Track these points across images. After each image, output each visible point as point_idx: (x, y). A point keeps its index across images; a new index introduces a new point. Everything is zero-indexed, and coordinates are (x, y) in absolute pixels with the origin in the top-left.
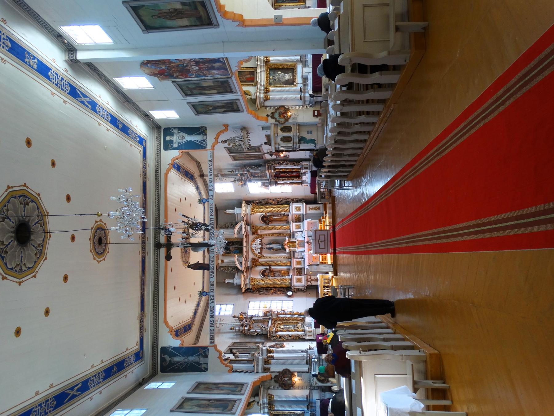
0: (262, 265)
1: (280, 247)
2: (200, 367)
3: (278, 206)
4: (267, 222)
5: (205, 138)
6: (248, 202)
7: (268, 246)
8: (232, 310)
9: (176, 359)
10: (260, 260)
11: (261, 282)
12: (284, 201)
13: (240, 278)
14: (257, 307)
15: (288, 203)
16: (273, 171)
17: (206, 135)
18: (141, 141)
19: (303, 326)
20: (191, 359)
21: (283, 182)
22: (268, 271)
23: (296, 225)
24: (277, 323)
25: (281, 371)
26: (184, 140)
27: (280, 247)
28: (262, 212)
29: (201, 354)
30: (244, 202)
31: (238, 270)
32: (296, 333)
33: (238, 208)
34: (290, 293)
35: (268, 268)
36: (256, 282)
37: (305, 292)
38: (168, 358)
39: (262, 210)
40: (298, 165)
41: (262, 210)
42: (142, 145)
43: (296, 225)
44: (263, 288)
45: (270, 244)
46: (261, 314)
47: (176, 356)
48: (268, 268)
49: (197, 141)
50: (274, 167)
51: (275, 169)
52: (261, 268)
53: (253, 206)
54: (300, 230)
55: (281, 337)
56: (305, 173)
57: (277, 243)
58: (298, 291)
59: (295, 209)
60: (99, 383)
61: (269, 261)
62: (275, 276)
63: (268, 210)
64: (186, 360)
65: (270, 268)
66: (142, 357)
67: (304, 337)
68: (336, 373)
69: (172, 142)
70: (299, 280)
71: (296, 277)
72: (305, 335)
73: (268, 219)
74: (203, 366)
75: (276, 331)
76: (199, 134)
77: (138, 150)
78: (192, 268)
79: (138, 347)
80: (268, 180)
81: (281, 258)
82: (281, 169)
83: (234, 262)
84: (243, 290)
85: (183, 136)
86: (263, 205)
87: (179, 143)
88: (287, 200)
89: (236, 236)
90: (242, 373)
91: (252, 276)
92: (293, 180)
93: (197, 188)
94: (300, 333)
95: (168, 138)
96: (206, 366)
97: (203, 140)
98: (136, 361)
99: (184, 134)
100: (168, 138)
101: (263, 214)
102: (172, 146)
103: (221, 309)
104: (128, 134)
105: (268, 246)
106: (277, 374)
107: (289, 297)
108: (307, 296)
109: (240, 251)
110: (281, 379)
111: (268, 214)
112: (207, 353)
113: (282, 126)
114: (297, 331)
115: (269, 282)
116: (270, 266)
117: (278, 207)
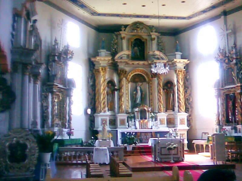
0: (120, 81)
1: (138, 101)
6: (187, 67)
7: (139, 88)
11: (102, 79)
12: (189, 106)
13: (106, 56)
14: (76, 72)
15: (187, 110)
27: (138, 101)
28: (178, 81)
32: (50, 117)
34: (89, 111)
36: (102, 73)
37: (90, 129)
43: (164, 119)
44: (94, 82)
52: (116, 80)
55: (46, 97)
57: (143, 99)
58: (91, 120)
61: (124, 90)
62: (108, 95)
65: (117, 90)
67: (45, 126)
68: (205, 171)
70: (104, 123)
72: (48, 127)
73: (169, 88)
81: (126, 103)
83: (122, 50)
84: (93, 59)
88: (190, 110)
89: (151, 53)
93: (204, 11)
94: (50, 121)
106: (9, 83)
107: (86, 112)
108: (87, 131)
109: (135, 58)
114: (53, 118)
115: (102, 88)
116: (119, 90)
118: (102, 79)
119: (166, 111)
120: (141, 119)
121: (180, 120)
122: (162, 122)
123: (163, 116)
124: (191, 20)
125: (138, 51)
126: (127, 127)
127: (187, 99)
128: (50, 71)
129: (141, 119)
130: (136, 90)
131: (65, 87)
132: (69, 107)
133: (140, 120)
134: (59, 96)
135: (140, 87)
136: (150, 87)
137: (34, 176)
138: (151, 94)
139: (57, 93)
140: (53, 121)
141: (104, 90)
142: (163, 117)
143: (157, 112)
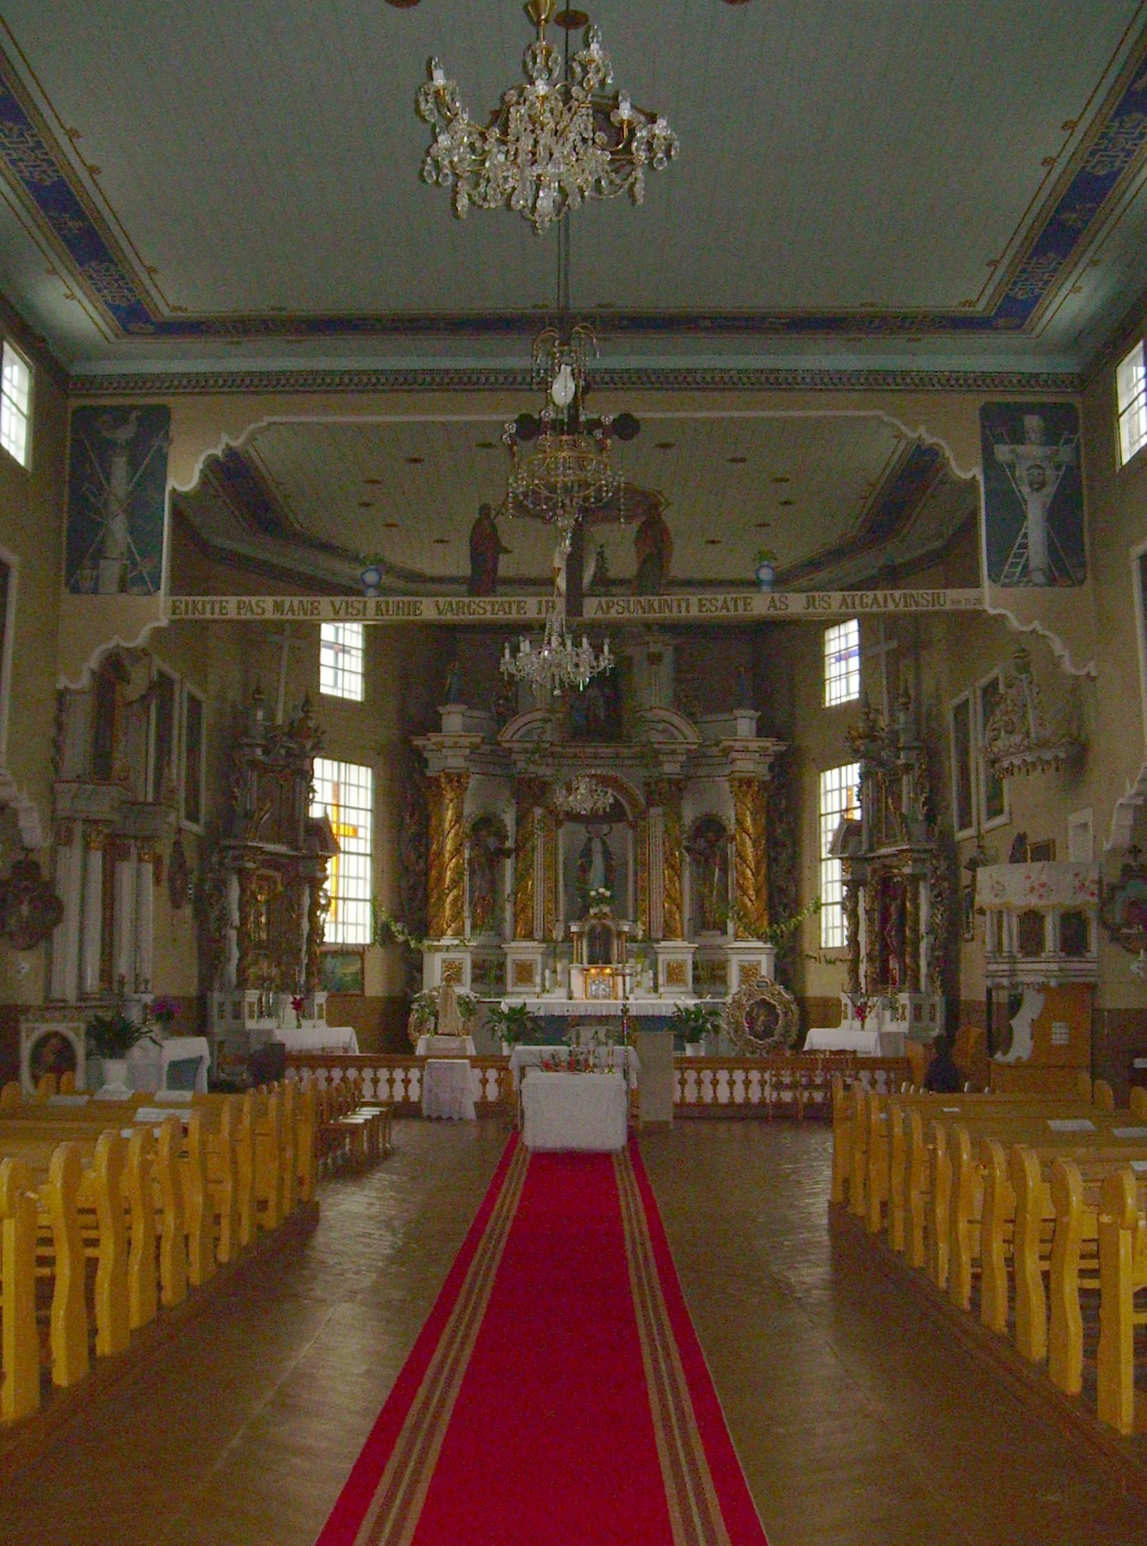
0: (519, 822)
2: (87, 562)
3: (764, 892)
4: (701, 843)
5: (1039, 577)
7: (597, 846)
8: (338, 693)
9: (120, 465)
10: (538, 812)
16: (907, 870)
17: (1052, 581)
18: (1014, 312)
19: (263, 982)
20: (118, 527)
21: (861, 912)
22: (492, 842)
23: (680, 966)
24: (278, 876)
25: (60, 892)
26: (1026, 490)
28: (740, 822)
29: (135, 565)
30: (782, 748)
31: (502, 719)
33: (759, 721)
35: (509, 844)
36: (449, 795)
38: (124, 434)
39: (749, 821)
40: (930, 977)
41: (749, 821)
42: (999, 314)
43: (680, 966)
45: (607, 856)
46: (316, 812)
47: (134, 463)
48: (509, 844)
49: (1024, 546)
50: (923, 877)
51: (915, 879)
53: (764, 786)
54: (661, 980)
56: (892, 1006)
59: (748, 956)
60: (13, 162)
63: (747, 848)
64: (114, 507)
66: (129, 333)
69: (1018, 437)
70: (452, 975)
71: (466, 960)
74: (87, 572)
75: (242, 873)
76: (1052, 550)
77: (972, 290)
78: (478, 525)
79: (167, 313)
80: (871, 848)
82: (917, 907)
84: (418, 742)
85: (1043, 485)
86: (769, 831)
87: (1012, 467)
90: (52, 732)
91: (473, 782)
92: (870, 957)
95: (1033, 422)
96: (87, 584)
97: (1026, 571)
98: (115, 308)
99: (1050, 490)
100: (1033, 422)
101: (732, 827)
102: (999, 440)
103: (344, 649)
104: (1039, 251)
105: (597, 846)
106: (45, 875)
110: (26, 889)
111: (731, 849)
112: (135, 590)
113: (1091, 915)
115: (449, 846)
117: (758, 891)
118: (450, 813)
119: (696, 934)
120: (592, 961)
121: (742, 968)
122: (674, 975)
123: (678, 950)
124: (151, 875)
125: (601, 702)
126: (538, 989)
127: (782, 891)
128: (236, 798)
129: (592, 961)
130: (587, 853)
131: (298, 849)
132: (310, 921)
133: (586, 966)
134: (275, 882)
135: (604, 843)
136: (641, 841)
137: (380, 1264)
138: (643, 865)
139: (262, 872)
140: (241, 971)
141: (457, 851)
142: (679, 957)
143: (660, 936)
